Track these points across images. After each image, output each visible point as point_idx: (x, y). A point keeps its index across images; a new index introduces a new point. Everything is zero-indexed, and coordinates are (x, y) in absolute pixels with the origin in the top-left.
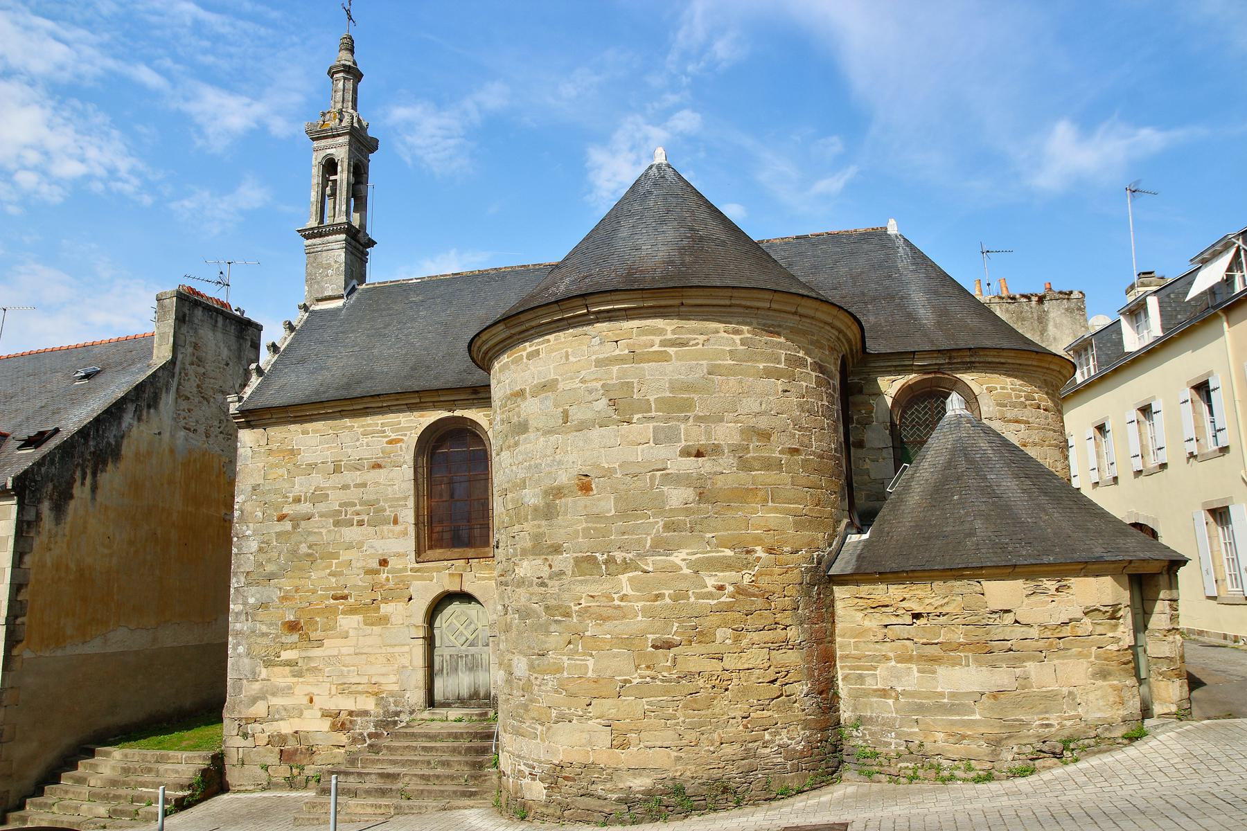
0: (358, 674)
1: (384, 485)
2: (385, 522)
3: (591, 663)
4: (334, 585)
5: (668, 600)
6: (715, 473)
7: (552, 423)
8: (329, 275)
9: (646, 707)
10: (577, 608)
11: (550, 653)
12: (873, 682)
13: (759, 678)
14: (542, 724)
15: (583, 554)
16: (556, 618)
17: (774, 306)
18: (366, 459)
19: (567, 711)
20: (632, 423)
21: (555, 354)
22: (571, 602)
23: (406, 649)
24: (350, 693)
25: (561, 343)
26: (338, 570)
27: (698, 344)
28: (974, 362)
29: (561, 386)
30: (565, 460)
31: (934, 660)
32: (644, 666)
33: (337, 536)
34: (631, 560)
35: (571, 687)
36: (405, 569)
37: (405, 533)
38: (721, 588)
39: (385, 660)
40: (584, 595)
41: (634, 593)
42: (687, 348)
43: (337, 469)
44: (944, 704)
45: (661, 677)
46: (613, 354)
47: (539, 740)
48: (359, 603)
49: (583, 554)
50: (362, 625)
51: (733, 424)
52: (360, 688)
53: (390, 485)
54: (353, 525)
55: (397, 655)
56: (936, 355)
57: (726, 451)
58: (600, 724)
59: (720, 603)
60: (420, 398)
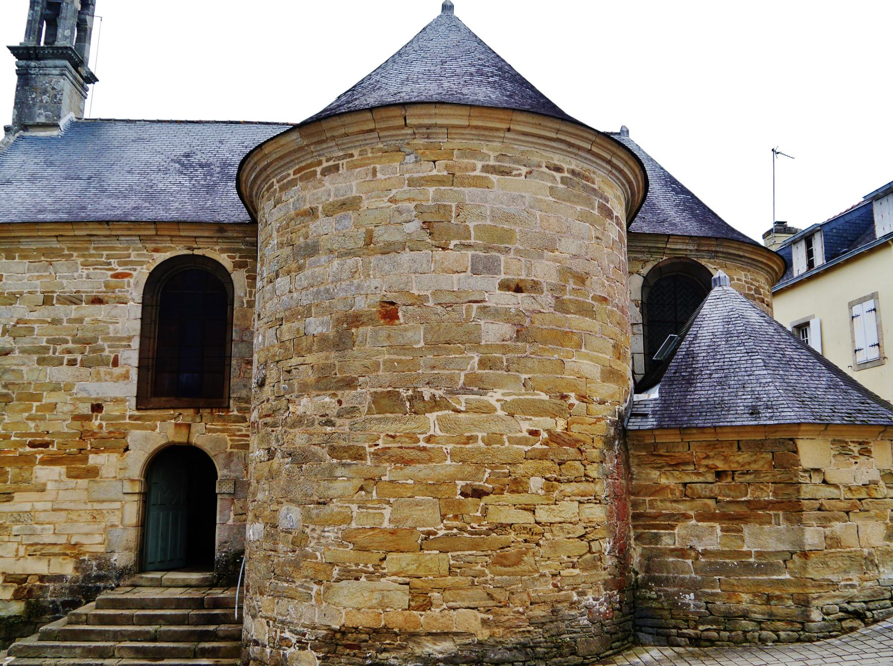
0: (54, 533)
1: (105, 322)
2: (103, 362)
3: (387, 511)
4: (33, 431)
5: (480, 443)
6: (533, 311)
7: (350, 245)
8: (44, 101)
9: (452, 562)
10: (372, 450)
11: (334, 500)
12: (670, 542)
13: (569, 533)
14: (320, 583)
15: (383, 389)
16: (344, 461)
17: (595, 149)
18: (84, 292)
19: (354, 568)
20: (448, 249)
21: (359, 169)
22: (365, 442)
23: (117, 505)
24: (43, 555)
25: (369, 158)
26: (39, 413)
27: (520, 175)
28: (717, 252)
29: (365, 204)
30: (366, 285)
31: (742, 518)
32: (451, 516)
33: (41, 376)
34: (441, 397)
35: (361, 539)
36: (123, 417)
37: (126, 376)
38: (534, 433)
39: (89, 518)
40: (382, 435)
41: (443, 434)
42: (509, 177)
43: (47, 301)
44: (751, 564)
45: (469, 529)
46: (430, 174)
47: (313, 602)
48: (63, 452)
49: (383, 389)
50: (64, 477)
51: (552, 263)
52: (56, 550)
53: (111, 323)
54: (62, 364)
55: (105, 512)
56: (687, 241)
57: (545, 289)
58: (395, 581)
59: (534, 449)
60: (156, 229)
